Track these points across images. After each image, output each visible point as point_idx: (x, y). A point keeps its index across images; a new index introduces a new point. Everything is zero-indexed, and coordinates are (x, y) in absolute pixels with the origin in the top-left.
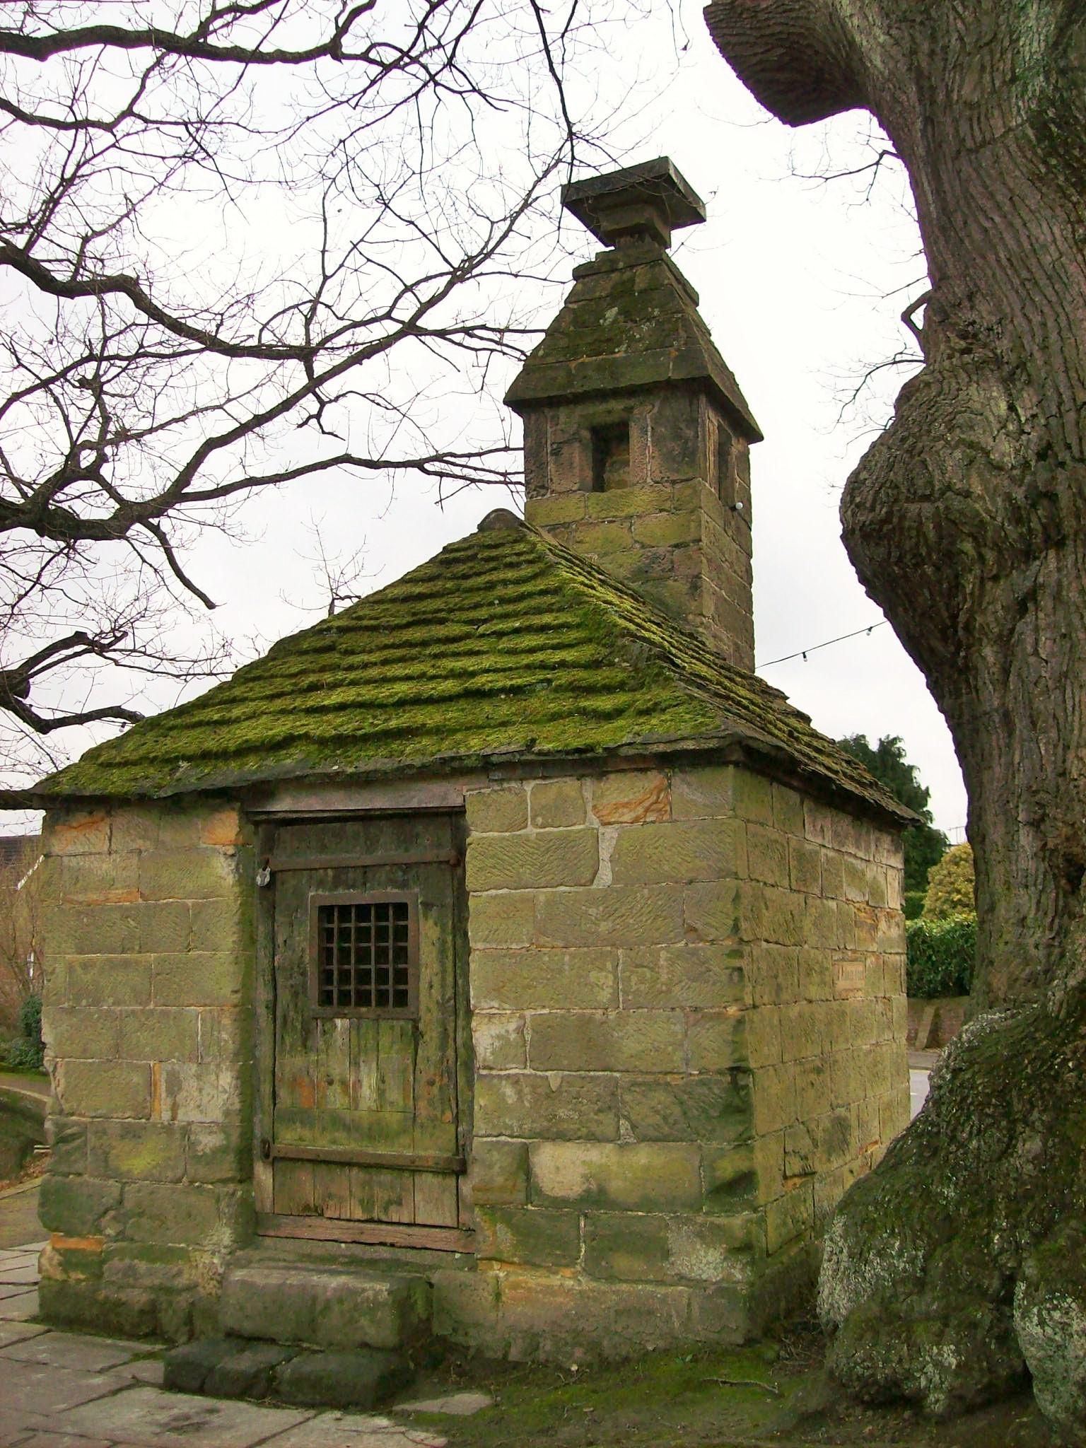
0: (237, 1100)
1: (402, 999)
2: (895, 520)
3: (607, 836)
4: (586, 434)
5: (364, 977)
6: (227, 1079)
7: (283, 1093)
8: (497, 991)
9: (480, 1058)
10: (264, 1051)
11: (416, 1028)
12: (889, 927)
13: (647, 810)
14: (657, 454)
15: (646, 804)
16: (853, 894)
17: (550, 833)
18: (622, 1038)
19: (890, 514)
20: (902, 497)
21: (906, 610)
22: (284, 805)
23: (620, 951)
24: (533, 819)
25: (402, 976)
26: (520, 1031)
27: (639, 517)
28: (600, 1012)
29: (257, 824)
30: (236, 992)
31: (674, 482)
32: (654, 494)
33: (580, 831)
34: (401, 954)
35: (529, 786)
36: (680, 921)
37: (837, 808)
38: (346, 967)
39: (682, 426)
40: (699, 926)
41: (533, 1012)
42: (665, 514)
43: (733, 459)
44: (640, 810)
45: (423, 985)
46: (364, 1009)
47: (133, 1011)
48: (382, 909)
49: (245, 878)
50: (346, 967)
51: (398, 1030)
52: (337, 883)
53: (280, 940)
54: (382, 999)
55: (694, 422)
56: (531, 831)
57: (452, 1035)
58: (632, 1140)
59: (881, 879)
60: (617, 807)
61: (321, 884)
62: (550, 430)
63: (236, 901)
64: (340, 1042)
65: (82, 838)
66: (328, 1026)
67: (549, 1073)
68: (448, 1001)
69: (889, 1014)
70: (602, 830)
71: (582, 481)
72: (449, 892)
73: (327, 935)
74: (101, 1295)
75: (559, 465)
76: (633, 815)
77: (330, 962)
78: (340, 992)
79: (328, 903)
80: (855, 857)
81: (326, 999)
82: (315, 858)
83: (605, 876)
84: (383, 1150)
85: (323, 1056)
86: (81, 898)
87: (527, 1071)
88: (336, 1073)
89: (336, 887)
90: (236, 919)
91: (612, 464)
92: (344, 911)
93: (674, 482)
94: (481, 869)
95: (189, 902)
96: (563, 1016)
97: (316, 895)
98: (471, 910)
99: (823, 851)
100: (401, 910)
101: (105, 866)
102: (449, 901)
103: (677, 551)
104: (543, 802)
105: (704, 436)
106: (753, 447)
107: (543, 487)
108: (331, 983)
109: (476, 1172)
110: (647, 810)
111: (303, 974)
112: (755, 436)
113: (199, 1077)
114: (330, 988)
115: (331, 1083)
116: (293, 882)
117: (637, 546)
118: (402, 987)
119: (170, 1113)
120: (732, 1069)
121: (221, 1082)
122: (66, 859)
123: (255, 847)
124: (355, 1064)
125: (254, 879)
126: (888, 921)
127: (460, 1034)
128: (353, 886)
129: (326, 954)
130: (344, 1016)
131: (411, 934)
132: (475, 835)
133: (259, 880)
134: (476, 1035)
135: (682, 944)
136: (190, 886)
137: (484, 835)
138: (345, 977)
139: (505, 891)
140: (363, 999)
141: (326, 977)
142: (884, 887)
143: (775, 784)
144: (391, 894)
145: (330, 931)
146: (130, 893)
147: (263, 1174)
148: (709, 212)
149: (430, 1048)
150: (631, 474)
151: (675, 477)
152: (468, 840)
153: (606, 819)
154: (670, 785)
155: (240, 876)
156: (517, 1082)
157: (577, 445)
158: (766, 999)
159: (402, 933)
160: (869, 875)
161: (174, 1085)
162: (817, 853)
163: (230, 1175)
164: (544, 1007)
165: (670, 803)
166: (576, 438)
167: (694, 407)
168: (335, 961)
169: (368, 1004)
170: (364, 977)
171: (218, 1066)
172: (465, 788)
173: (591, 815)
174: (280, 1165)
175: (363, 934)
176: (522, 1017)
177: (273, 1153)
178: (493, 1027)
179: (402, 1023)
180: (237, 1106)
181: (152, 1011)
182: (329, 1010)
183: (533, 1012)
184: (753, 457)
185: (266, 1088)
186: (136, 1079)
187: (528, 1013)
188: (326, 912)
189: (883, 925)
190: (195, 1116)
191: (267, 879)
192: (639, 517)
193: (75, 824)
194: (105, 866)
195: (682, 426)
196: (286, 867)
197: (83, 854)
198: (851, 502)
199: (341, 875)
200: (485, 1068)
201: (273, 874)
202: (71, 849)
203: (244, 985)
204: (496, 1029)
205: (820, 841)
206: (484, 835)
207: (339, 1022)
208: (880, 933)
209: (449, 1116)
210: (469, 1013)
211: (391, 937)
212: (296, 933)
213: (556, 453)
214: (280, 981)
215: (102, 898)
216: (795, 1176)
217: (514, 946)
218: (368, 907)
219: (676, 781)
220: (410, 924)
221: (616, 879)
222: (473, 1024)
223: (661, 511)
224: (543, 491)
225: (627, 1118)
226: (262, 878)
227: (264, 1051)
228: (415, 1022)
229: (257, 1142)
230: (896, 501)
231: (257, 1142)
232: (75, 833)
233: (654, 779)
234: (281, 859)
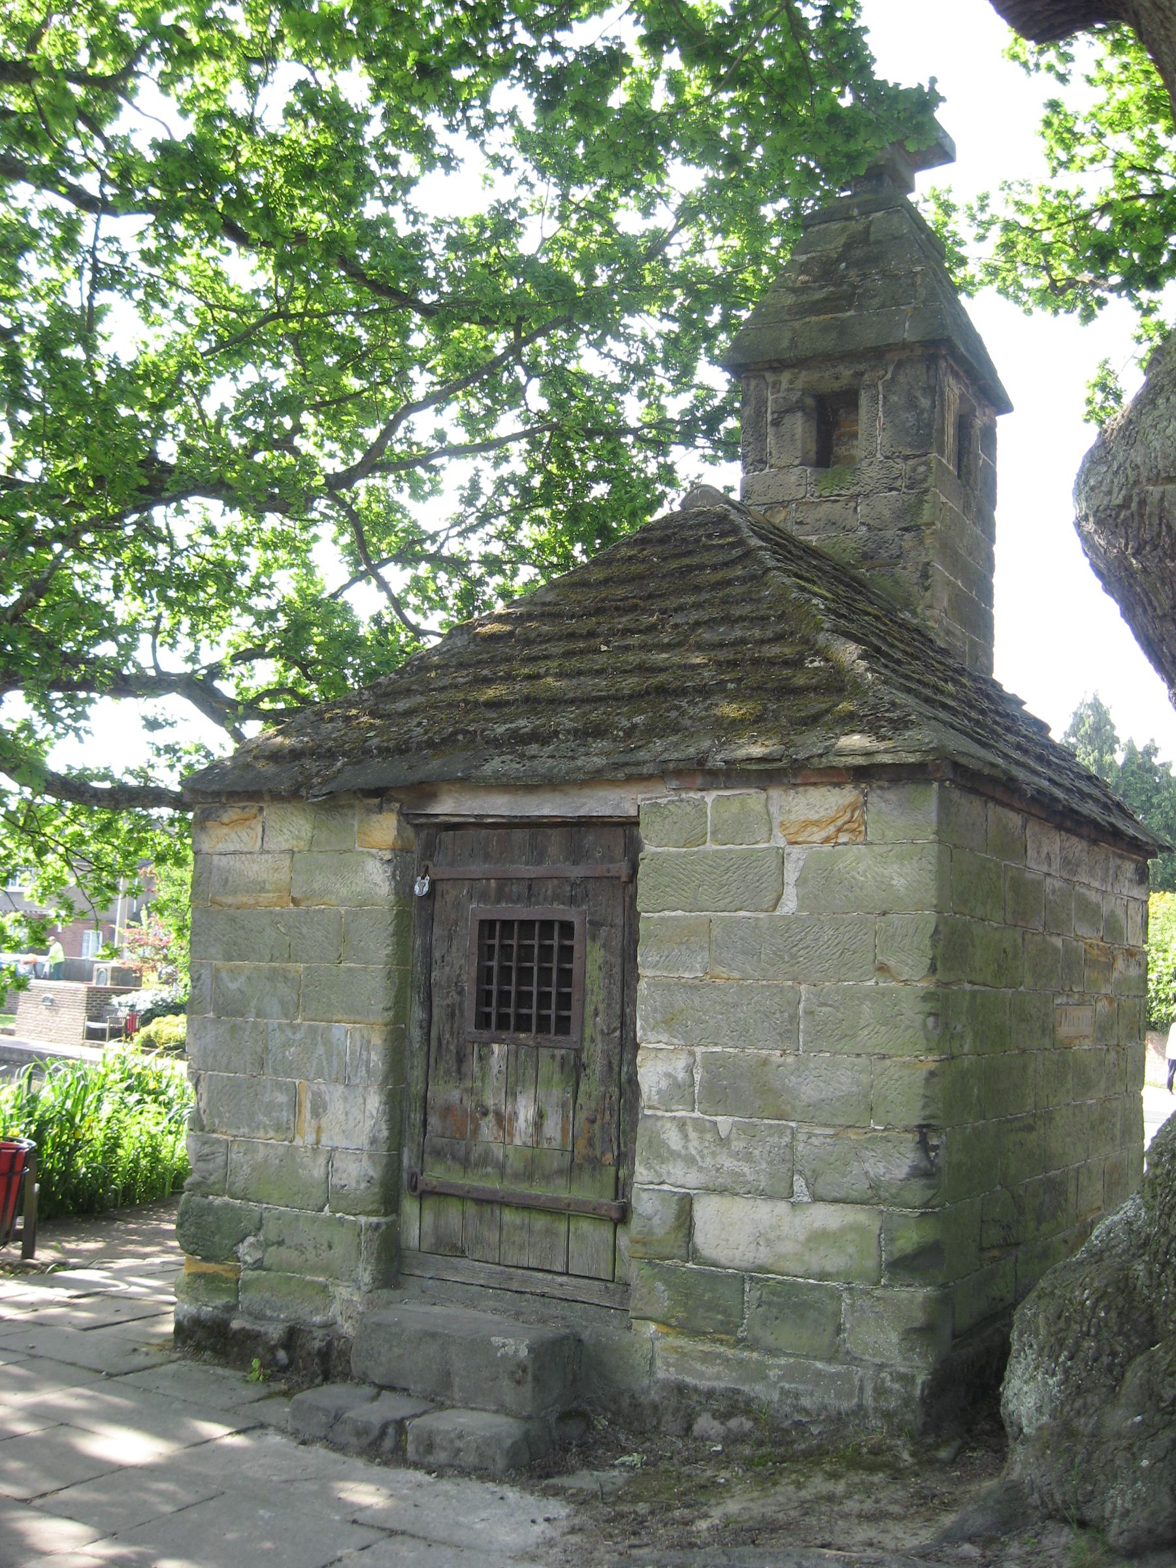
0: (384, 1127)
1: (564, 1025)
2: (1134, 506)
3: (794, 856)
4: (810, 402)
5: (524, 999)
6: (374, 1102)
7: (433, 1120)
8: (668, 1021)
9: (645, 1096)
10: (416, 1074)
11: (578, 1057)
12: (1128, 966)
13: (839, 830)
14: (888, 426)
15: (839, 823)
16: (1084, 930)
17: (730, 851)
18: (800, 1084)
19: (1128, 500)
20: (1143, 479)
21: (1145, 611)
22: (447, 806)
23: (803, 987)
24: (714, 833)
25: (565, 1001)
26: (690, 1070)
27: (867, 496)
28: (778, 1053)
29: (418, 828)
30: (387, 1009)
31: (906, 458)
32: (883, 471)
33: (763, 850)
34: (566, 976)
35: (710, 797)
36: (871, 957)
37: (1069, 831)
38: (507, 988)
39: (918, 394)
40: (892, 963)
41: (704, 1049)
42: (894, 493)
43: (976, 431)
44: (831, 829)
45: (589, 1009)
46: (522, 1035)
47: (280, 1025)
48: (547, 925)
49: (403, 889)
50: (507, 988)
51: (558, 1058)
52: (501, 896)
53: (437, 955)
54: (543, 1025)
55: (934, 391)
56: (711, 846)
57: (616, 1069)
58: (806, 1199)
59: (1120, 912)
60: (807, 824)
61: (484, 897)
62: (770, 398)
63: (391, 910)
64: (495, 1071)
65: (233, 836)
66: (485, 1051)
67: (719, 1118)
68: (615, 1030)
69: (1123, 1064)
70: (788, 849)
71: (805, 453)
72: (620, 910)
73: (486, 952)
74: (235, 1325)
75: (779, 436)
76: (824, 834)
77: (489, 981)
78: (559, 994)
79: (490, 917)
80: (1088, 886)
81: (483, 1021)
82: (477, 868)
83: (790, 904)
84: (538, 1190)
85: (479, 1084)
86: (230, 900)
87: (697, 1114)
88: (490, 1102)
89: (498, 901)
90: (391, 929)
91: (839, 438)
92: (507, 925)
93: (906, 458)
94: (654, 888)
95: (343, 910)
96: (736, 1056)
97: (477, 910)
98: (641, 932)
99: (1049, 880)
100: (567, 928)
101: (256, 868)
102: (619, 921)
103: (908, 536)
104: (726, 816)
105: (942, 406)
106: (999, 419)
107: (761, 461)
108: (489, 1004)
109: (635, 1224)
110: (839, 830)
111: (461, 993)
112: (1002, 405)
113: (345, 1099)
114: (487, 1010)
115: (485, 1114)
116: (453, 893)
117: (864, 528)
118: (565, 1013)
119: (314, 1136)
120: (920, 1127)
121: (369, 1107)
122: (216, 858)
123: (417, 849)
124: (511, 1094)
125: (412, 888)
126: (1126, 960)
127: (625, 1069)
128: (519, 899)
129: (485, 975)
130: (500, 1042)
131: (576, 955)
132: (650, 847)
133: (417, 888)
134: (641, 1071)
135: (872, 982)
136: (344, 892)
137: (659, 850)
138: (504, 997)
139: (680, 913)
140: (523, 1024)
141: (484, 997)
142: (1123, 923)
143: (991, 805)
144: (558, 911)
145: (492, 947)
146: (280, 897)
147: (410, 1207)
148: (959, 153)
149: (592, 1085)
150: (859, 449)
151: (908, 452)
152: (641, 856)
153: (793, 838)
154: (865, 803)
155: (397, 883)
156: (684, 1124)
157: (799, 414)
158: (966, 1049)
159: (567, 952)
160: (1105, 910)
161: (319, 1109)
162: (1039, 883)
163: (370, 1207)
164: (716, 1044)
165: (865, 824)
166: (799, 406)
167: (932, 372)
168: (495, 981)
169: (529, 1030)
170: (524, 999)
171: (365, 1088)
172: (640, 796)
173: (777, 832)
174: (428, 1203)
175: (526, 952)
176: (692, 1054)
177: (420, 1187)
178: (659, 1063)
179: (563, 1052)
180: (385, 1133)
181: (299, 1025)
182: (486, 1034)
183: (704, 1049)
184: (1001, 432)
185: (416, 1117)
186: (282, 1098)
187: (699, 1050)
188: (487, 927)
189: (1120, 964)
190: (340, 1141)
191: (426, 889)
192: (867, 496)
193: (226, 819)
194: (256, 868)
195: (918, 394)
196: (445, 876)
197: (234, 853)
198: (1085, 483)
199: (503, 888)
200: (650, 1108)
201: (433, 884)
202: (221, 847)
203: (396, 1003)
204: (662, 1067)
205: (1045, 869)
206: (659, 850)
207: (496, 1047)
208: (1116, 974)
209: (609, 1158)
210: (637, 1047)
211: (555, 956)
212: (454, 949)
213: (776, 423)
214: (436, 1001)
215: (252, 901)
216: (993, 1247)
217: (686, 975)
218: (532, 923)
219: (873, 798)
220: (576, 943)
221: (800, 907)
222: (639, 1059)
223: (891, 490)
224: (761, 466)
225: (801, 1173)
226: (421, 887)
227: (416, 1074)
228: (578, 1052)
229: (405, 1176)
230: (1136, 482)
231: (405, 1176)
232: (225, 830)
233: (847, 795)
234: (441, 871)
